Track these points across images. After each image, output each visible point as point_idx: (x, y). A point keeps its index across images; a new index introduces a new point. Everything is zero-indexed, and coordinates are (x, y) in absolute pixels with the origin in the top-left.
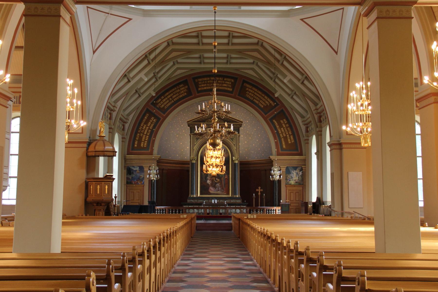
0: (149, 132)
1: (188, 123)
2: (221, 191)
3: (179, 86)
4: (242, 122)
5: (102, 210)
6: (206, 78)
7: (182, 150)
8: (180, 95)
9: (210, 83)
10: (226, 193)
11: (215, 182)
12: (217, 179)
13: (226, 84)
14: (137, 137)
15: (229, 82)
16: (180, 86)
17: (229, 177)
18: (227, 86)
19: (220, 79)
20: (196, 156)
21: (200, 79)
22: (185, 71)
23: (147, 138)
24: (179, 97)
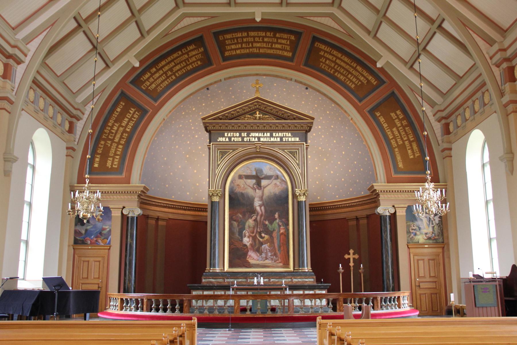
0: (124, 138)
1: (203, 121)
2: (272, 259)
3: (187, 49)
4: (313, 119)
7: (198, 184)
8: (187, 65)
9: (248, 43)
10: (281, 264)
11: (259, 240)
12: (263, 235)
13: (281, 44)
14: (101, 148)
16: (189, 49)
17: (287, 230)
18: (281, 48)
19: (268, 34)
20: (220, 189)
22: (199, 19)
23: (120, 150)
24: (185, 68)
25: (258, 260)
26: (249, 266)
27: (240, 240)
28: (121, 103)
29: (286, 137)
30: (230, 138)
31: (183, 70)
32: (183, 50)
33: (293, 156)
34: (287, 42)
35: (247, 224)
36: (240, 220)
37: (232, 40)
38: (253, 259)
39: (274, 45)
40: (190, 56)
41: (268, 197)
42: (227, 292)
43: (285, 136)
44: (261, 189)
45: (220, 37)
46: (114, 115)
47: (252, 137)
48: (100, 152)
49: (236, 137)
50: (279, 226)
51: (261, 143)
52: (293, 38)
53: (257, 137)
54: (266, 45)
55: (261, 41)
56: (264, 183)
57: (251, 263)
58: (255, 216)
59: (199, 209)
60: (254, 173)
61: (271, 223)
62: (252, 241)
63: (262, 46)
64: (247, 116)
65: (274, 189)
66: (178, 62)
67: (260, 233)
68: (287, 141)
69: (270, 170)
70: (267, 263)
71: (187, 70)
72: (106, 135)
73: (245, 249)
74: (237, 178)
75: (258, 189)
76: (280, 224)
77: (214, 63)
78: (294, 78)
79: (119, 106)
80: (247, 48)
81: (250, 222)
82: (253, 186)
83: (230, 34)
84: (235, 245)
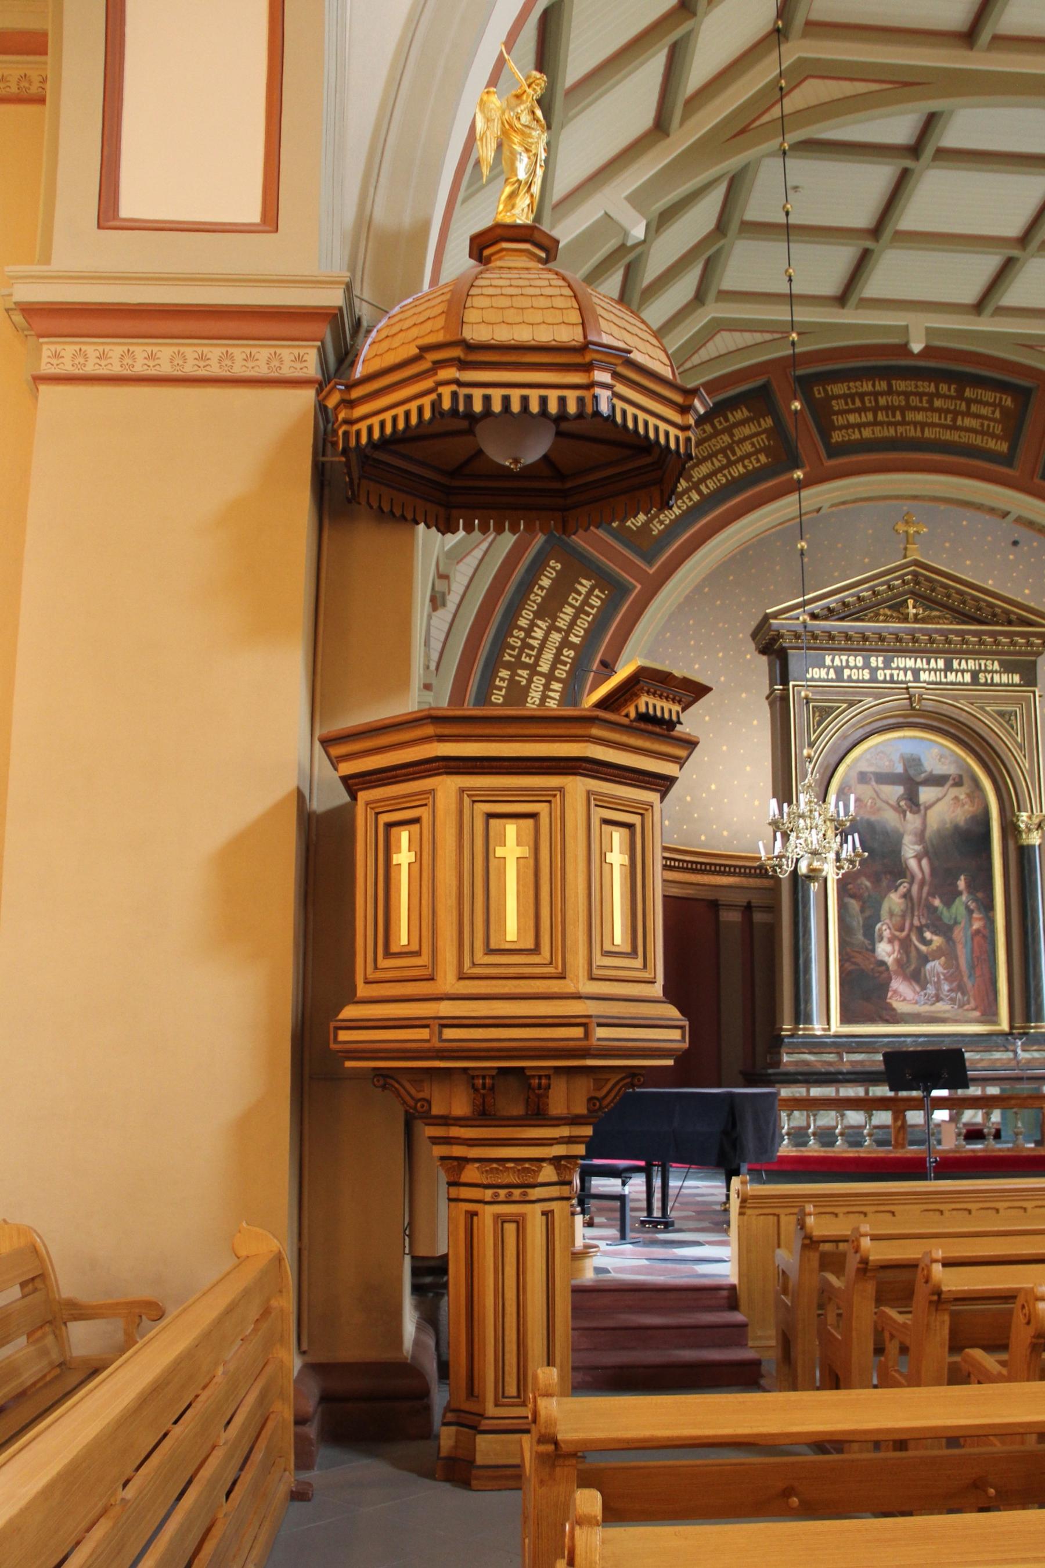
0: (565, 664)
2: (953, 1000)
3: (727, 420)
5: (548, 1173)
6: (870, 384)
7: (688, 798)
8: (730, 464)
9: (889, 409)
10: (976, 1014)
11: (917, 949)
12: (928, 935)
13: (977, 416)
14: (500, 689)
15: (991, 409)
16: (732, 419)
17: (991, 922)
18: (980, 428)
19: (944, 388)
21: (840, 385)
22: (758, 337)
23: (556, 695)
24: (726, 472)
25: (916, 1003)
26: (895, 1018)
27: (867, 950)
28: (552, 563)
29: (986, 671)
30: (839, 671)
31: (719, 476)
32: (716, 421)
33: (1007, 722)
34: (993, 412)
35: (885, 907)
36: (866, 894)
37: (849, 401)
38: (904, 1000)
39: (960, 418)
40: (736, 439)
41: (938, 831)
42: (871, 1089)
43: (983, 667)
44: (918, 812)
45: (815, 389)
46: (532, 597)
47: (898, 668)
48: (500, 702)
49: (856, 667)
50: (970, 912)
51: (924, 685)
52: (1008, 402)
53: (910, 669)
54: (940, 419)
55: (927, 405)
56: (926, 794)
57: (899, 1011)
58: (906, 884)
59: (708, 868)
60: (899, 769)
61: (948, 903)
62: (899, 951)
63: (930, 421)
64: (882, 611)
65: (954, 812)
66: (706, 454)
67: (920, 931)
68: (989, 681)
69: (940, 760)
70: (939, 1012)
71: (730, 478)
72: (512, 652)
73: (881, 973)
74: (853, 781)
75: (911, 812)
76: (972, 907)
77: (806, 462)
78: (1016, 512)
79: (545, 573)
80: (889, 424)
81: (894, 900)
82: (898, 804)
83: (842, 383)
84: (855, 963)
